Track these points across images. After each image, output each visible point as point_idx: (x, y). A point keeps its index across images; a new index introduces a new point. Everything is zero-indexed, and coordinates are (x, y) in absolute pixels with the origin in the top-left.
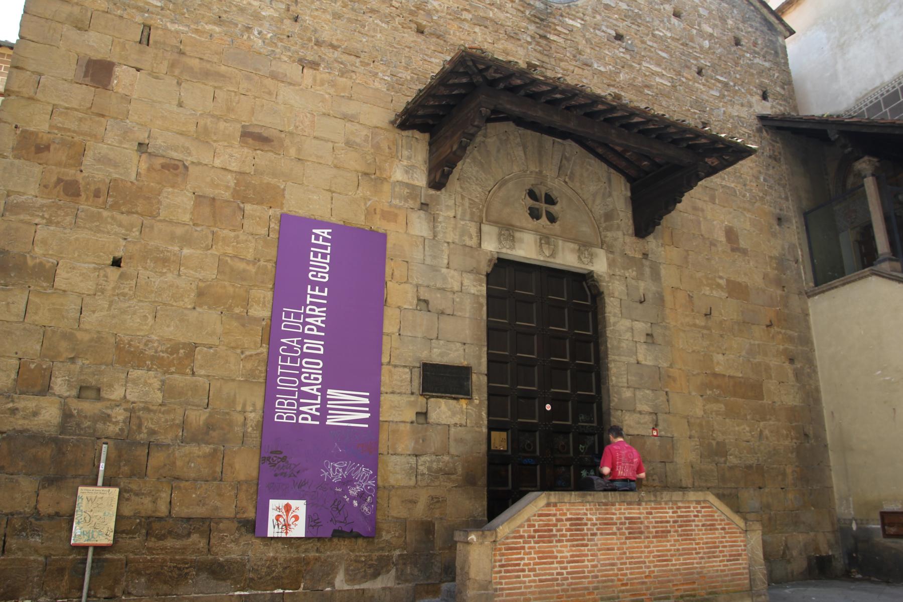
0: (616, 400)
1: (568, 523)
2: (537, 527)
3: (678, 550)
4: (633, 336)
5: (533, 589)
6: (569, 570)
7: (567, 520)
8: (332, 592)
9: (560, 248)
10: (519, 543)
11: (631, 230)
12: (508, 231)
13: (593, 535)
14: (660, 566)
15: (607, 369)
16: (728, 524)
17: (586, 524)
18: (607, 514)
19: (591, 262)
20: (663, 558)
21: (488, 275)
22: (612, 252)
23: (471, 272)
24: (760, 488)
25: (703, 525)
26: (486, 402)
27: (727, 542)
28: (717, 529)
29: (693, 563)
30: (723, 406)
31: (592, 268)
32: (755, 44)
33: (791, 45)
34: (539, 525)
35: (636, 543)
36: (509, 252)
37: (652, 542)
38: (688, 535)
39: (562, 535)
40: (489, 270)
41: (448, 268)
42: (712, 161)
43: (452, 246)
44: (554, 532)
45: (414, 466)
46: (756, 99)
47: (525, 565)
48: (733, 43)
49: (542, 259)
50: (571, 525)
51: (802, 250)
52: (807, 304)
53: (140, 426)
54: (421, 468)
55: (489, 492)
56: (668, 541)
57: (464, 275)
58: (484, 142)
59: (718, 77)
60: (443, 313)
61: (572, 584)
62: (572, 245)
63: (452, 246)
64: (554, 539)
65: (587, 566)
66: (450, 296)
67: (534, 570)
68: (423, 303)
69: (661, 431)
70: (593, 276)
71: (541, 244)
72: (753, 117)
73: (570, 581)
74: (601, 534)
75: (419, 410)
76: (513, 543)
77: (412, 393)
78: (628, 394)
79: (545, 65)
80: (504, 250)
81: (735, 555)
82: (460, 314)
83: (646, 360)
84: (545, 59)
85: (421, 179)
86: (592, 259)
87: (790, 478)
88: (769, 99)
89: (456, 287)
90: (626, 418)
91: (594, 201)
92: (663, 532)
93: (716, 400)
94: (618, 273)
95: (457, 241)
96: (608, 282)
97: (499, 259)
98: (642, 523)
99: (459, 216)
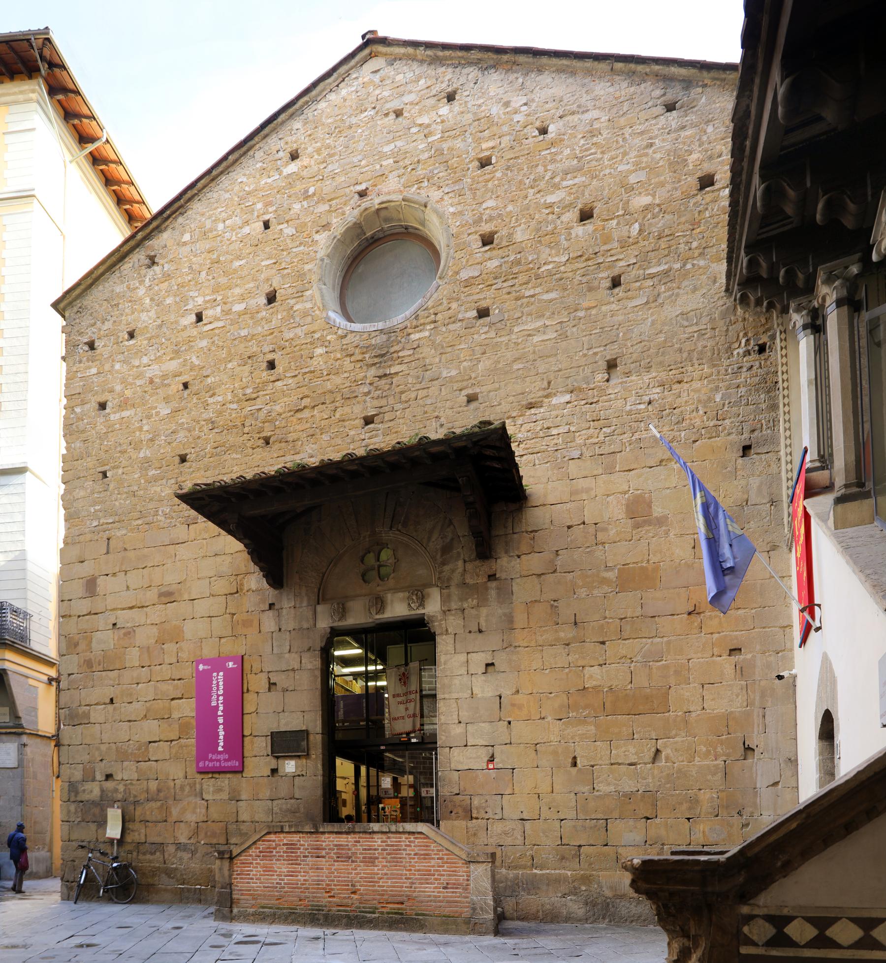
0: (443, 738)
1: (285, 847)
3: (386, 874)
13: (304, 857)
14: (366, 886)
16: (446, 855)
17: (299, 849)
27: (444, 871)
29: (402, 887)
30: (593, 727)
36: (340, 624)
37: (359, 866)
38: (397, 862)
40: (323, 644)
43: (293, 632)
53: (130, 793)
57: (303, 654)
62: (401, 595)
63: (293, 632)
64: (274, 859)
66: (291, 674)
67: (259, 879)
69: (497, 763)
73: (286, 889)
78: (458, 730)
79: (382, 410)
80: (335, 624)
84: (383, 402)
90: (455, 754)
91: (429, 539)
92: (371, 858)
93: (583, 721)
94: (455, 607)
96: (441, 620)
98: (349, 849)
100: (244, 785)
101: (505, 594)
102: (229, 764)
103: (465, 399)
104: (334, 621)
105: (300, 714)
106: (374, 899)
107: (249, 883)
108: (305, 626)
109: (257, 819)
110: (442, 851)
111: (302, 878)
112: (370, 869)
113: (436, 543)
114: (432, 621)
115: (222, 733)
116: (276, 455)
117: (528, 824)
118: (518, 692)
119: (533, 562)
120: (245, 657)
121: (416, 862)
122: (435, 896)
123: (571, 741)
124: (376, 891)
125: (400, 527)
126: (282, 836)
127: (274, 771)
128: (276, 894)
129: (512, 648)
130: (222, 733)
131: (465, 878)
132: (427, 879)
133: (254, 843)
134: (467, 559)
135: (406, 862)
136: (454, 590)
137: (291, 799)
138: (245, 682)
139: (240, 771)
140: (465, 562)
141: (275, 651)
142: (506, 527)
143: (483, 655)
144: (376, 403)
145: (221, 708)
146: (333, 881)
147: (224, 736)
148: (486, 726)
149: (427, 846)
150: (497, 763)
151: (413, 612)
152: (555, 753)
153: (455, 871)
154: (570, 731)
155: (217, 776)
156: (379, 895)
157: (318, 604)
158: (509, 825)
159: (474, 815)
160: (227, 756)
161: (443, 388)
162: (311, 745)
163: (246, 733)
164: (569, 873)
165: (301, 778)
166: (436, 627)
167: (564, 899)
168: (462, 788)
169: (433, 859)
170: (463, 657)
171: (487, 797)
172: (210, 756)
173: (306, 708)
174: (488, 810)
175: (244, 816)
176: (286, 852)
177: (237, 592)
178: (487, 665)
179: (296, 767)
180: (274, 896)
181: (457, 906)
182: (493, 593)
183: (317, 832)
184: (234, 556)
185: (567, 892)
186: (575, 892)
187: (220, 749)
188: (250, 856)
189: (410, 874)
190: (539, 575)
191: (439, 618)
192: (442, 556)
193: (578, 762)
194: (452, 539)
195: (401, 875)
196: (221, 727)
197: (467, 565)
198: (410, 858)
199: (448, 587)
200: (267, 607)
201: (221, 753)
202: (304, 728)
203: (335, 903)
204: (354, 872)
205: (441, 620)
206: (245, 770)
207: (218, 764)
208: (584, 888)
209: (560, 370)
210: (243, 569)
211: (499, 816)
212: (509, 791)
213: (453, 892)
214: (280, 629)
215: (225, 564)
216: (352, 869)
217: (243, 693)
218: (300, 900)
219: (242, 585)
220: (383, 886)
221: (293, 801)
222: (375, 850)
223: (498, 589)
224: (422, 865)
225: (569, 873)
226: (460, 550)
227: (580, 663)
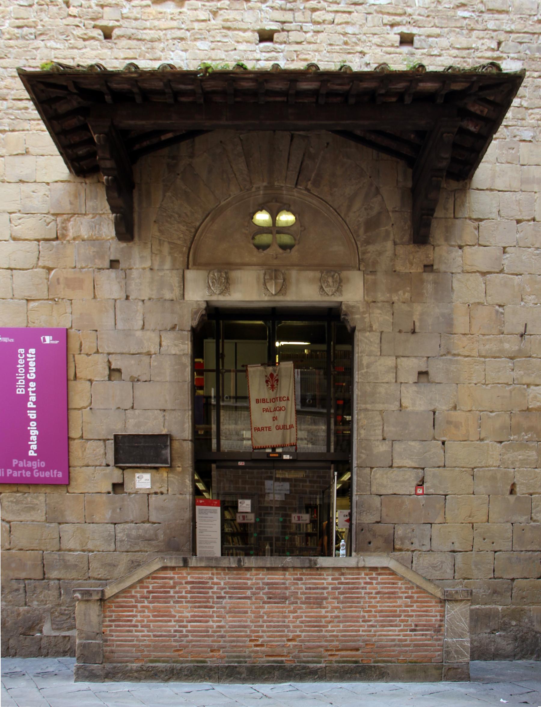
2: (151, 589)
5: (147, 643)
6: (189, 628)
9: (293, 280)
10: (132, 602)
17: (211, 588)
20: (317, 624)
23: (173, 328)
27: (412, 611)
30: (534, 453)
34: (153, 587)
35: (277, 607)
36: (221, 298)
37: (300, 608)
43: (148, 303)
44: (172, 594)
45: (113, 533)
47: (137, 621)
49: (266, 298)
57: (163, 334)
58: (190, 165)
61: (191, 641)
62: (311, 274)
63: (148, 303)
65: (212, 627)
66: (146, 359)
68: (114, 373)
73: (190, 638)
74: (230, 598)
75: (116, 481)
76: (124, 602)
77: (108, 465)
78: (382, 448)
79: (286, 26)
80: (214, 298)
82: (158, 379)
83: (414, 404)
84: (288, 16)
85: (108, 230)
90: (378, 476)
91: (349, 207)
92: (317, 598)
93: (523, 446)
95: (153, 297)
96: (364, 313)
99: (156, 267)
100: (69, 503)
101: (443, 290)
102: (47, 474)
103: (398, 38)
104: (212, 294)
105: (160, 414)
106: (321, 647)
108: (168, 295)
109: (90, 546)
110: (412, 588)
111: (215, 625)
112: (314, 612)
113: (357, 215)
114: (352, 313)
115: (34, 433)
116: (122, 56)
117: (459, 556)
118: (455, 408)
119: (477, 257)
120: (72, 332)
121: (378, 602)
122: (400, 640)
123: (511, 466)
124: (324, 636)
125: (309, 186)
126: (184, 572)
127: (118, 487)
128: (174, 644)
129: (449, 357)
130: (34, 433)
131: (439, 618)
132: (391, 621)
133: (141, 581)
134: (398, 241)
135: (365, 602)
136: (382, 279)
137: (143, 522)
138: (71, 365)
139: (65, 483)
140: (395, 244)
141: (120, 326)
142: (446, 209)
143: (415, 360)
144: (279, 15)
145: (33, 398)
146: (262, 626)
147: (38, 437)
148: (415, 445)
149: (393, 584)
150: (428, 488)
151: (326, 298)
152: (493, 478)
153: (426, 611)
154: (510, 456)
155: (25, 489)
156: (326, 641)
157: (188, 268)
158: (436, 559)
159: (397, 547)
160: (43, 464)
161: (370, 17)
162: (175, 456)
163: (73, 434)
164: (500, 608)
165: (159, 496)
166: (356, 320)
167: (492, 635)
168: (384, 515)
169: (400, 598)
170: (390, 362)
171: (414, 526)
172: (15, 462)
173: (169, 406)
174: (415, 540)
175: (70, 543)
176: (190, 592)
177: (57, 238)
178: (420, 373)
179: (153, 482)
180: (172, 646)
181: (426, 651)
182: (429, 287)
183: (239, 568)
184: (52, 186)
185: (496, 628)
186: (504, 627)
187: (31, 453)
188: (132, 597)
189: (369, 616)
190: (484, 274)
191: (361, 310)
192: (366, 232)
193: (517, 489)
194: (379, 213)
195: (358, 617)
196: (33, 424)
197: (398, 248)
198: (371, 598)
199: (373, 273)
200: (107, 264)
201: (32, 459)
202: (164, 432)
203: (263, 652)
204: (292, 615)
205: (364, 313)
206: (73, 483)
207: (28, 474)
208: (514, 623)
209: (511, 32)
210: (67, 208)
211: (428, 548)
212: (439, 519)
213: (423, 635)
214: (127, 298)
215: (40, 199)
216: (290, 612)
217: (68, 380)
218: (212, 651)
219: (65, 228)
220: (333, 631)
221: (147, 525)
222: (324, 588)
223: (435, 283)
224: (387, 605)
225: (500, 608)
226: (389, 227)
227: (526, 380)
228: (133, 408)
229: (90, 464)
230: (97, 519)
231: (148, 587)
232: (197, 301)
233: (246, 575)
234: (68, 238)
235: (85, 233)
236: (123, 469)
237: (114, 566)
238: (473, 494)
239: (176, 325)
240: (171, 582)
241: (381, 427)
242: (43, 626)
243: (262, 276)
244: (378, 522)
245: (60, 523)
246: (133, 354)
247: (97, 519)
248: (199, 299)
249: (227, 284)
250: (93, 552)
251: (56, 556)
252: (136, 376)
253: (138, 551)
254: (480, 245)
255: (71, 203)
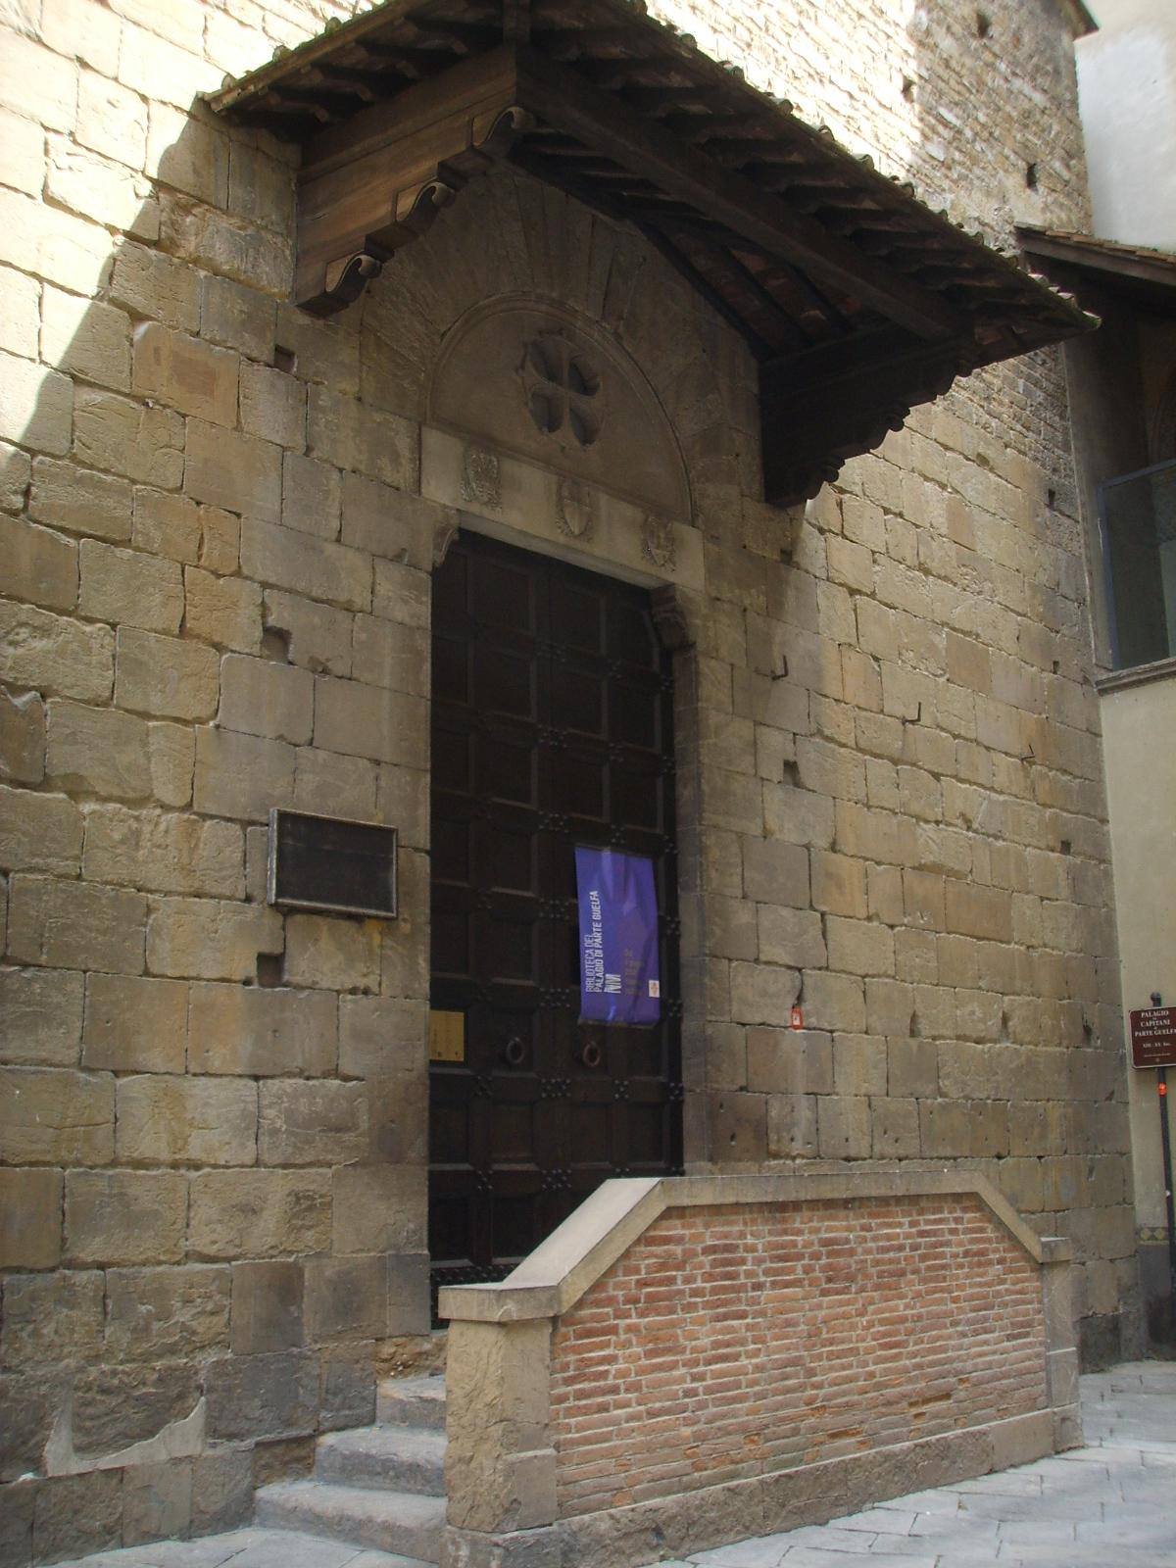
0: (718, 931)
2: (643, 1275)
4: (756, 766)
7: (707, 1251)
8: (37, 1489)
11: (757, 488)
12: (484, 447)
14: (886, 1359)
15: (702, 850)
17: (743, 1261)
18: (785, 1232)
19: (671, 560)
21: (436, 573)
22: (715, 539)
23: (398, 558)
24: (999, 1157)
25: (966, 1254)
26: (428, 929)
28: (990, 1263)
31: (672, 578)
32: (1017, 40)
33: (1087, 54)
36: (487, 512)
39: (695, 1293)
40: (441, 557)
41: (338, 541)
42: (985, 334)
46: (1015, 181)
48: (975, 29)
49: (562, 539)
50: (715, 1264)
51: (1090, 574)
52: (1097, 707)
54: (271, 1113)
55: (436, 1181)
56: (901, 1297)
59: (943, 111)
60: (325, 671)
70: (672, 599)
71: (560, 498)
72: (1009, 228)
75: (266, 949)
80: (475, 508)
81: (1022, 1325)
86: (672, 552)
87: (1054, 1139)
88: (1041, 188)
89: (361, 599)
92: (891, 1274)
95: (362, 467)
97: (461, 531)
98: (852, 1252)
107: (603, 1408)
109: (194, 1152)
123: (909, 979)
137: (326, 1075)
151: (653, 570)
191: (704, 611)
214: (309, 450)
228: (311, 743)
229: (207, 888)
230: (217, 1063)
231: (637, 1271)
232: (445, 506)
233: (794, 1222)
234: (182, 253)
235: (222, 254)
236: (288, 912)
237: (254, 1212)
238: (866, 1033)
239: (404, 550)
240: (678, 1250)
241: (739, 870)
242: (47, 1439)
243: (554, 487)
244: (742, 1089)
245: (116, 1074)
246: (316, 600)
247: (217, 1063)
248: (448, 503)
249: (494, 484)
250: (197, 1167)
251: (102, 1185)
252: (322, 659)
253: (310, 1164)
254: (845, 537)
255: (196, 171)
